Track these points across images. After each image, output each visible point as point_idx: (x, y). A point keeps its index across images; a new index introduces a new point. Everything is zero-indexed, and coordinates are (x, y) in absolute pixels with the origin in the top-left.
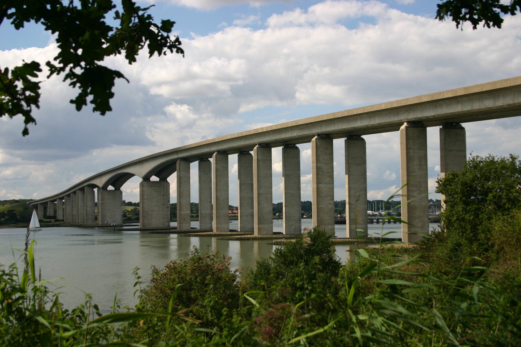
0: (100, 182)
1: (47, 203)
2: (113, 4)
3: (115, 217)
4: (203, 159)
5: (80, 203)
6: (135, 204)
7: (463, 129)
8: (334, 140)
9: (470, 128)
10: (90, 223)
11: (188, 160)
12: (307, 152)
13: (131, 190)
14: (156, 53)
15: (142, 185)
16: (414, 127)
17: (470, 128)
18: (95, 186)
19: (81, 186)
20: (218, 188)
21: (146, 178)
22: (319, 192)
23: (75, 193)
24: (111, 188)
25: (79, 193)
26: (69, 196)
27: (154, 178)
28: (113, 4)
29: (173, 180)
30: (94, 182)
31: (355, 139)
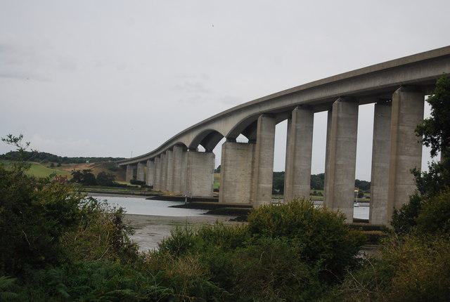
1: (136, 164)
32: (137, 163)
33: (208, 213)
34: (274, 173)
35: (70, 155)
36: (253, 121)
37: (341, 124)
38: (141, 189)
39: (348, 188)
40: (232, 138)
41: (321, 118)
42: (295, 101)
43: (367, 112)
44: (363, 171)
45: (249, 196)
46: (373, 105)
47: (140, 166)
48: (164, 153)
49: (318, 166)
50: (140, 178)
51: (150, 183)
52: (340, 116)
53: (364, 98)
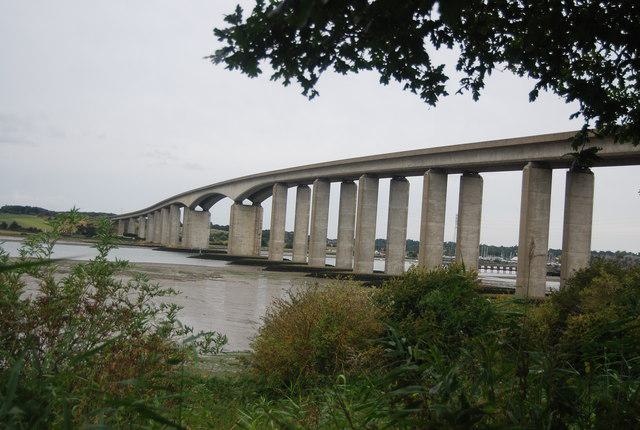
0: (188, 202)
1: (128, 219)
2: (392, 78)
3: (200, 239)
4: (302, 185)
5: (165, 223)
6: (222, 228)
7: (592, 174)
8: (554, 170)
9: (487, 177)
10: (173, 244)
11: (286, 185)
12: (416, 183)
13: (221, 213)
14: (282, 79)
15: (233, 207)
16: (539, 168)
17: (487, 177)
18: (181, 205)
19: (167, 204)
20: (298, 219)
21: (238, 201)
22: (425, 230)
23: (159, 210)
24: (199, 208)
25: (164, 211)
26: (152, 213)
27: (247, 202)
28: (392, 78)
29: (267, 204)
30: (180, 201)
31: (471, 175)
32: (126, 219)
33: (266, 270)
34: (481, 246)
35: (50, 209)
36: (260, 189)
37: (366, 195)
38: (133, 240)
39: (369, 245)
40: (192, 208)
41: (292, 191)
42: (315, 174)
43: (292, 191)
44: (332, 234)
45: (252, 249)
46: (460, 175)
47: (131, 221)
48: (159, 210)
49: (450, 234)
50: (132, 230)
51: (142, 236)
52: (365, 188)
53: (336, 179)
